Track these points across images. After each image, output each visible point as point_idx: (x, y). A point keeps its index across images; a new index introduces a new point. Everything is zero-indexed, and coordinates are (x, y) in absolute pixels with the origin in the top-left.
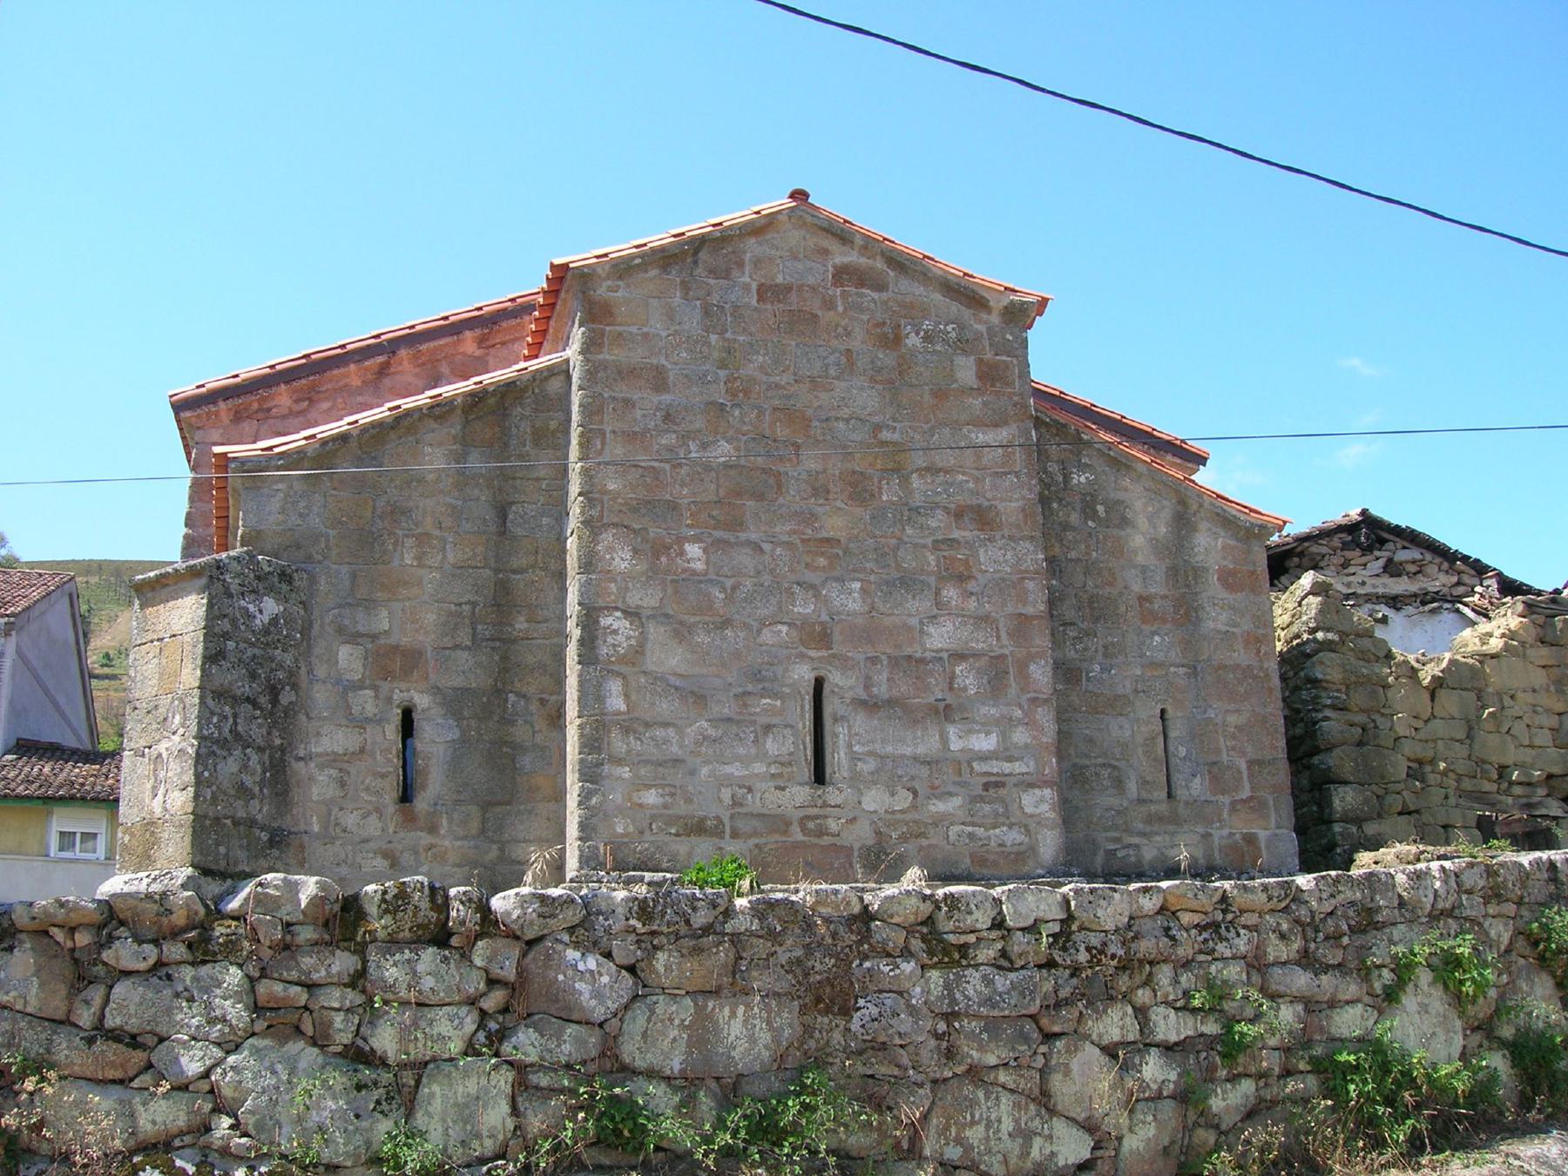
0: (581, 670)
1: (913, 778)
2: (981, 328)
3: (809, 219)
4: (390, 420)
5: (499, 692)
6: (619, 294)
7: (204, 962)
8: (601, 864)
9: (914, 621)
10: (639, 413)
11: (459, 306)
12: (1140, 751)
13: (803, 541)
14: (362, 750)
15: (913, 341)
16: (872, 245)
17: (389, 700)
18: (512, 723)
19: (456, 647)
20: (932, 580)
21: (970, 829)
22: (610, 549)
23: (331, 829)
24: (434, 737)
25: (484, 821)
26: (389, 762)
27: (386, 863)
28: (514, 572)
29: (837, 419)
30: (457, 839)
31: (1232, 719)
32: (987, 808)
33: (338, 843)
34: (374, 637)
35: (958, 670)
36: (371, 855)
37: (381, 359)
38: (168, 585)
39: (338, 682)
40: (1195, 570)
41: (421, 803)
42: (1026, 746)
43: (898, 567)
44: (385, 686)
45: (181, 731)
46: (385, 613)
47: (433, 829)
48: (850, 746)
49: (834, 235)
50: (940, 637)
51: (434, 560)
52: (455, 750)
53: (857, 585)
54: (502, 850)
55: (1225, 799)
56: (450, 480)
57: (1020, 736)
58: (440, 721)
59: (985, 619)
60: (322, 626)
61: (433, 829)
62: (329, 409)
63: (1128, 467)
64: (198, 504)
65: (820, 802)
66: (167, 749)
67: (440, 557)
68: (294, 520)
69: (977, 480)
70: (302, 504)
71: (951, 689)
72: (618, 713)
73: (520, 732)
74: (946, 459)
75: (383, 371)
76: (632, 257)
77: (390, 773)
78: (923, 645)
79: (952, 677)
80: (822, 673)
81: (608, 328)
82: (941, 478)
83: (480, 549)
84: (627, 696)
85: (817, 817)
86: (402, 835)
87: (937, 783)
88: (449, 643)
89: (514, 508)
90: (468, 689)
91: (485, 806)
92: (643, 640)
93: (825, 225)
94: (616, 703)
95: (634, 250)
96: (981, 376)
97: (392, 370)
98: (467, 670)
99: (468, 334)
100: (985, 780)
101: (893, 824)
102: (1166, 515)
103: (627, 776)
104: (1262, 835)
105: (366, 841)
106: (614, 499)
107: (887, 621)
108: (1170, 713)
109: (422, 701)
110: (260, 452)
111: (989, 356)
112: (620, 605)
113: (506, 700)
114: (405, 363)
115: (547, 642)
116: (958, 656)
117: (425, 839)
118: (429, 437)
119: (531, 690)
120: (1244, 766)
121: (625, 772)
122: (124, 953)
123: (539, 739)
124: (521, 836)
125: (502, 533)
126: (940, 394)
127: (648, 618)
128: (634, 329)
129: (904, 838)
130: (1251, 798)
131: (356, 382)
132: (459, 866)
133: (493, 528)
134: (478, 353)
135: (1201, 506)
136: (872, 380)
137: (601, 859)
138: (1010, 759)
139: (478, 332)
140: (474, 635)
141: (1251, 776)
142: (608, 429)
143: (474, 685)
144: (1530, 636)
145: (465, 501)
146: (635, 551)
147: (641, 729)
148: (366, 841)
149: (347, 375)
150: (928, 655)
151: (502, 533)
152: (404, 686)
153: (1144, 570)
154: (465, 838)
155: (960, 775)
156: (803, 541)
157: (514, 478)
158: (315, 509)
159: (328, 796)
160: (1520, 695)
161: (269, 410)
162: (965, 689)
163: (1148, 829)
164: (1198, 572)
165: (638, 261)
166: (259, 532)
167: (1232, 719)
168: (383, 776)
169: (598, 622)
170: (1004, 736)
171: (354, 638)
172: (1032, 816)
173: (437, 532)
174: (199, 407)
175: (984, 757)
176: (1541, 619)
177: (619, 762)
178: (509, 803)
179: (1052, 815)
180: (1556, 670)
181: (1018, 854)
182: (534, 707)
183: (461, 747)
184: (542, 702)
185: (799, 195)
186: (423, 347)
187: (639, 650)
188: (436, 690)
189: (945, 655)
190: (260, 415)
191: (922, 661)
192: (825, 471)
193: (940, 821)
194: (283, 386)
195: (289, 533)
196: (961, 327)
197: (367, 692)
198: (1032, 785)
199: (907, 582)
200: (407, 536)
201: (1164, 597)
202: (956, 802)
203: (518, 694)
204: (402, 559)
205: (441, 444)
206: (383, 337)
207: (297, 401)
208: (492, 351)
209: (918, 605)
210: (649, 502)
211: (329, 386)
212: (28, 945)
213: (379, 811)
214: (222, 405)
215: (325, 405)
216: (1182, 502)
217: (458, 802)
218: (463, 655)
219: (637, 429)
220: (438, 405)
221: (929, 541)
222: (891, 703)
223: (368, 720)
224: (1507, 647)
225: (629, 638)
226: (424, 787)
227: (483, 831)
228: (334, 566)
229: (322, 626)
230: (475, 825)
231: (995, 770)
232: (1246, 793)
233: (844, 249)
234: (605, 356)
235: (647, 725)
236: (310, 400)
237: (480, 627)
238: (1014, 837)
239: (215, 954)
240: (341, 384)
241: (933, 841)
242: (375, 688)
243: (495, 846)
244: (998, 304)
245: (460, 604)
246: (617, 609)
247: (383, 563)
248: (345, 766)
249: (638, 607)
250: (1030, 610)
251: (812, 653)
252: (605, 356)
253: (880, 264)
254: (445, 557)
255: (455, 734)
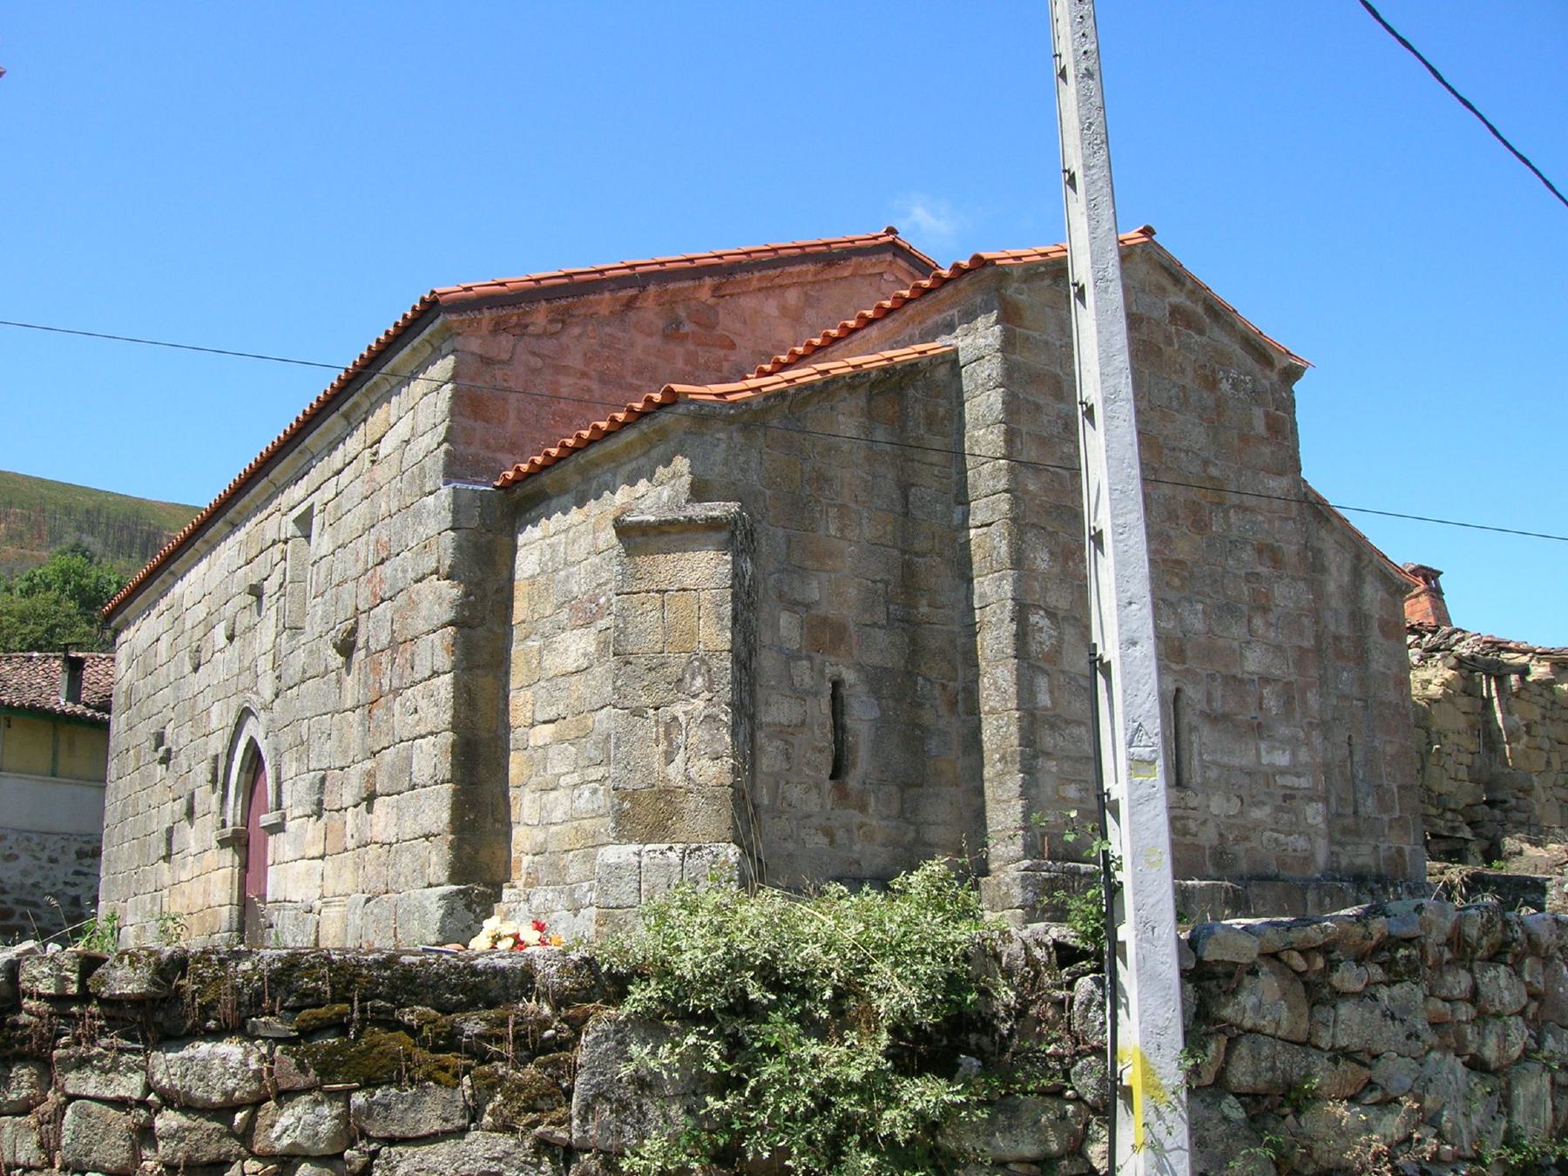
0: (1018, 664)
1: (1240, 787)
2: (1266, 383)
3: (1155, 256)
4: (820, 383)
5: (910, 675)
6: (1023, 297)
7: (1394, 983)
8: (1039, 853)
9: (1235, 644)
10: (1045, 419)
11: (704, 248)
12: (1337, 770)
13: (1163, 560)
14: (803, 723)
15: (1225, 386)
16: (1198, 290)
17: (822, 673)
18: (920, 705)
19: (874, 625)
20: (1245, 608)
21: (1276, 835)
22: (1034, 549)
23: (779, 802)
24: (862, 714)
25: (903, 802)
26: (822, 736)
27: (827, 840)
28: (916, 554)
29: (1181, 450)
30: (883, 819)
31: (1389, 749)
32: (1286, 816)
33: (784, 817)
34: (808, 606)
35: (1265, 691)
36: (813, 831)
37: (632, 292)
38: (669, 533)
39: (781, 650)
40: (1365, 615)
41: (853, 781)
42: (1306, 764)
43: (1225, 595)
44: (818, 658)
45: (707, 695)
46: (815, 584)
47: (863, 808)
48: (1201, 755)
49: (1170, 274)
50: (1254, 661)
51: (852, 534)
52: (877, 729)
53: (1200, 607)
54: (917, 831)
55: (1386, 818)
56: (862, 454)
57: (1304, 755)
58: (864, 698)
59: (1279, 648)
60: (765, 589)
61: (863, 808)
62: (580, 336)
63: (1328, 520)
64: (458, 418)
65: (1183, 805)
66: (685, 713)
67: (857, 531)
68: (737, 474)
69: (1270, 522)
70: (742, 459)
71: (1261, 708)
72: (1046, 709)
73: (927, 717)
74: (1251, 502)
75: (630, 304)
76: (1037, 264)
77: (825, 748)
78: (1242, 666)
79: (1261, 699)
80: (1180, 684)
81: (1018, 330)
82: (1248, 516)
83: (889, 528)
84: (1051, 692)
85: (1182, 818)
86: (837, 811)
87: (1254, 792)
88: (867, 619)
89: (913, 490)
90: (885, 669)
91: (904, 786)
92: (1060, 640)
93: (1167, 264)
94: (1044, 699)
95: (1039, 258)
96: (1269, 427)
97: (638, 304)
98: (883, 649)
99: (708, 281)
100: (1283, 792)
101: (1230, 827)
102: (1348, 565)
103: (1054, 769)
104: (1407, 849)
105: (809, 816)
106: (1032, 499)
107: (1220, 642)
108: (1354, 740)
109: (849, 676)
110: (714, 398)
111: (1272, 410)
112: (1042, 603)
113: (916, 684)
114: (650, 299)
115: (945, 628)
116: (1265, 680)
117: (858, 817)
118: (841, 406)
119: (934, 675)
120: (1396, 790)
121: (1052, 765)
122: (1348, 977)
123: (941, 723)
124: (932, 818)
125: (906, 514)
126: (1244, 439)
127: (1063, 618)
128: (1036, 334)
129: (1236, 841)
130: (1401, 817)
131: (604, 310)
132: (884, 845)
133: (898, 508)
134: (711, 301)
135: (1371, 562)
136: (1200, 417)
137: (1040, 848)
138: (1298, 775)
139: (716, 280)
140: (888, 614)
141: (1400, 798)
142: (1024, 430)
143: (890, 665)
144: (1459, 685)
145: (874, 477)
146: (1051, 553)
147: (1063, 726)
148: (809, 816)
149: (599, 303)
150: (1246, 676)
151: (906, 514)
152: (833, 659)
153: (1336, 611)
154: (888, 818)
155: (1268, 787)
156: (1163, 560)
157: (913, 460)
158: (753, 465)
159: (776, 769)
160: (1450, 734)
161: (526, 326)
162: (1270, 710)
163: (1343, 839)
164: (1367, 618)
165: (1042, 269)
166: (706, 482)
167: (1389, 749)
168: (821, 751)
169: (1028, 619)
170: (1294, 754)
171: (793, 605)
172: (1312, 826)
173: (853, 505)
174: (465, 311)
175: (1283, 772)
176: (1465, 673)
177: (1048, 755)
178: (921, 786)
179: (1322, 826)
180: (1471, 717)
181: (1306, 859)
182: (937, 692)
183: (883, 725)
184: (944, 687)
185: (1148, 231)
186: (671, 286)
187: (1057, 650)
188: (860, 667)
189: (1256, 677)
190: (518, 331)
191: (1241, 681)
192: (1174, 498)
193: (1258, 826)
194: (544, 303)
195: (733, 488)
196: (1254, 380)
197: (804, 662)
198: (1311, 799)
199: (1229, 609)
200: (830, 505)
201: (1348, 638)
202: (1267, 810)
203: (925, 678)
204: (827, 529)
205: (852, 415)
206: (638, 269)
207: (552, 321)
208: (722, 301)
209: (1238, 630)
210: (1058, 507)
211: (582, 311)
212: (1265, 969)
213: (817, 786)
214: (486, 313)
215: (576, 331)
216: (1358, 557)
217: (882, 782)
218: (880, 635)
219: (1045, 434)
220: (858, 375)
221: (1242, 573)
222: (1226, 717)
223: (807, 692)
224: (1445, 694)
225: (1051, 637)
226: (854, 765)
227: (902, 811)
228: (772, 529)
229: (765, 589)
230: (896, 805)
231: (1289, 784)
232: (1397, 814)
233: (1175, 289)
234: (1016, 357)
235: (1068, 722)
236: (563, 322)
237: (891, 607)
238: (1302, 843)
239: (1401, 975)
240: (591, 311)
241: (1253, 844)
242: (810, 659)
243: (912, 827)
244: (1281, 363)
245: (874, 582)
246: (1040, 607)
247: (813, 531)
248: (790, 738)
249: (1056, 607)
250: (1306, 644)
251: (1174, 666)
252: (1016, 357)
253: (1200, 310)
254: (861, 531)
255: (876, 713)
